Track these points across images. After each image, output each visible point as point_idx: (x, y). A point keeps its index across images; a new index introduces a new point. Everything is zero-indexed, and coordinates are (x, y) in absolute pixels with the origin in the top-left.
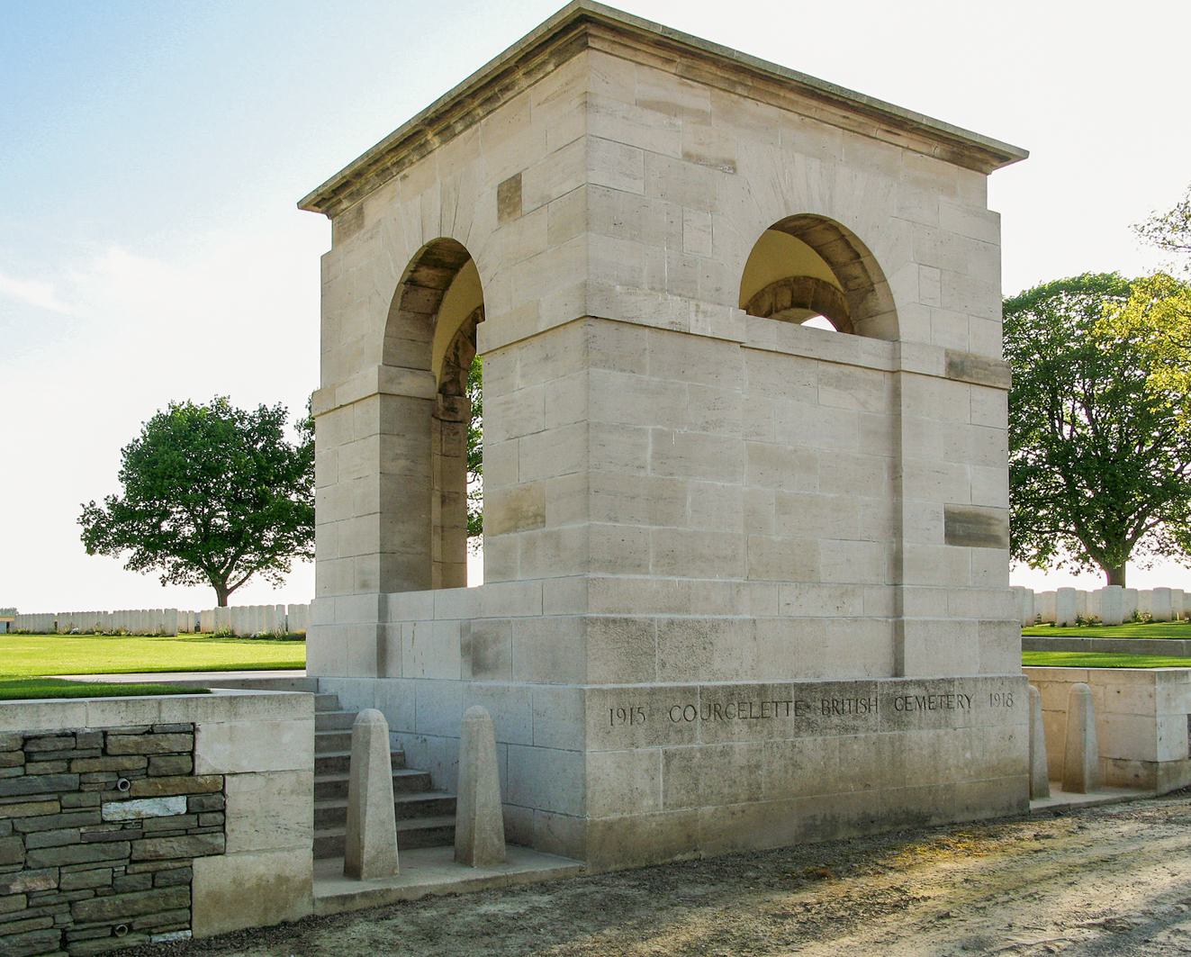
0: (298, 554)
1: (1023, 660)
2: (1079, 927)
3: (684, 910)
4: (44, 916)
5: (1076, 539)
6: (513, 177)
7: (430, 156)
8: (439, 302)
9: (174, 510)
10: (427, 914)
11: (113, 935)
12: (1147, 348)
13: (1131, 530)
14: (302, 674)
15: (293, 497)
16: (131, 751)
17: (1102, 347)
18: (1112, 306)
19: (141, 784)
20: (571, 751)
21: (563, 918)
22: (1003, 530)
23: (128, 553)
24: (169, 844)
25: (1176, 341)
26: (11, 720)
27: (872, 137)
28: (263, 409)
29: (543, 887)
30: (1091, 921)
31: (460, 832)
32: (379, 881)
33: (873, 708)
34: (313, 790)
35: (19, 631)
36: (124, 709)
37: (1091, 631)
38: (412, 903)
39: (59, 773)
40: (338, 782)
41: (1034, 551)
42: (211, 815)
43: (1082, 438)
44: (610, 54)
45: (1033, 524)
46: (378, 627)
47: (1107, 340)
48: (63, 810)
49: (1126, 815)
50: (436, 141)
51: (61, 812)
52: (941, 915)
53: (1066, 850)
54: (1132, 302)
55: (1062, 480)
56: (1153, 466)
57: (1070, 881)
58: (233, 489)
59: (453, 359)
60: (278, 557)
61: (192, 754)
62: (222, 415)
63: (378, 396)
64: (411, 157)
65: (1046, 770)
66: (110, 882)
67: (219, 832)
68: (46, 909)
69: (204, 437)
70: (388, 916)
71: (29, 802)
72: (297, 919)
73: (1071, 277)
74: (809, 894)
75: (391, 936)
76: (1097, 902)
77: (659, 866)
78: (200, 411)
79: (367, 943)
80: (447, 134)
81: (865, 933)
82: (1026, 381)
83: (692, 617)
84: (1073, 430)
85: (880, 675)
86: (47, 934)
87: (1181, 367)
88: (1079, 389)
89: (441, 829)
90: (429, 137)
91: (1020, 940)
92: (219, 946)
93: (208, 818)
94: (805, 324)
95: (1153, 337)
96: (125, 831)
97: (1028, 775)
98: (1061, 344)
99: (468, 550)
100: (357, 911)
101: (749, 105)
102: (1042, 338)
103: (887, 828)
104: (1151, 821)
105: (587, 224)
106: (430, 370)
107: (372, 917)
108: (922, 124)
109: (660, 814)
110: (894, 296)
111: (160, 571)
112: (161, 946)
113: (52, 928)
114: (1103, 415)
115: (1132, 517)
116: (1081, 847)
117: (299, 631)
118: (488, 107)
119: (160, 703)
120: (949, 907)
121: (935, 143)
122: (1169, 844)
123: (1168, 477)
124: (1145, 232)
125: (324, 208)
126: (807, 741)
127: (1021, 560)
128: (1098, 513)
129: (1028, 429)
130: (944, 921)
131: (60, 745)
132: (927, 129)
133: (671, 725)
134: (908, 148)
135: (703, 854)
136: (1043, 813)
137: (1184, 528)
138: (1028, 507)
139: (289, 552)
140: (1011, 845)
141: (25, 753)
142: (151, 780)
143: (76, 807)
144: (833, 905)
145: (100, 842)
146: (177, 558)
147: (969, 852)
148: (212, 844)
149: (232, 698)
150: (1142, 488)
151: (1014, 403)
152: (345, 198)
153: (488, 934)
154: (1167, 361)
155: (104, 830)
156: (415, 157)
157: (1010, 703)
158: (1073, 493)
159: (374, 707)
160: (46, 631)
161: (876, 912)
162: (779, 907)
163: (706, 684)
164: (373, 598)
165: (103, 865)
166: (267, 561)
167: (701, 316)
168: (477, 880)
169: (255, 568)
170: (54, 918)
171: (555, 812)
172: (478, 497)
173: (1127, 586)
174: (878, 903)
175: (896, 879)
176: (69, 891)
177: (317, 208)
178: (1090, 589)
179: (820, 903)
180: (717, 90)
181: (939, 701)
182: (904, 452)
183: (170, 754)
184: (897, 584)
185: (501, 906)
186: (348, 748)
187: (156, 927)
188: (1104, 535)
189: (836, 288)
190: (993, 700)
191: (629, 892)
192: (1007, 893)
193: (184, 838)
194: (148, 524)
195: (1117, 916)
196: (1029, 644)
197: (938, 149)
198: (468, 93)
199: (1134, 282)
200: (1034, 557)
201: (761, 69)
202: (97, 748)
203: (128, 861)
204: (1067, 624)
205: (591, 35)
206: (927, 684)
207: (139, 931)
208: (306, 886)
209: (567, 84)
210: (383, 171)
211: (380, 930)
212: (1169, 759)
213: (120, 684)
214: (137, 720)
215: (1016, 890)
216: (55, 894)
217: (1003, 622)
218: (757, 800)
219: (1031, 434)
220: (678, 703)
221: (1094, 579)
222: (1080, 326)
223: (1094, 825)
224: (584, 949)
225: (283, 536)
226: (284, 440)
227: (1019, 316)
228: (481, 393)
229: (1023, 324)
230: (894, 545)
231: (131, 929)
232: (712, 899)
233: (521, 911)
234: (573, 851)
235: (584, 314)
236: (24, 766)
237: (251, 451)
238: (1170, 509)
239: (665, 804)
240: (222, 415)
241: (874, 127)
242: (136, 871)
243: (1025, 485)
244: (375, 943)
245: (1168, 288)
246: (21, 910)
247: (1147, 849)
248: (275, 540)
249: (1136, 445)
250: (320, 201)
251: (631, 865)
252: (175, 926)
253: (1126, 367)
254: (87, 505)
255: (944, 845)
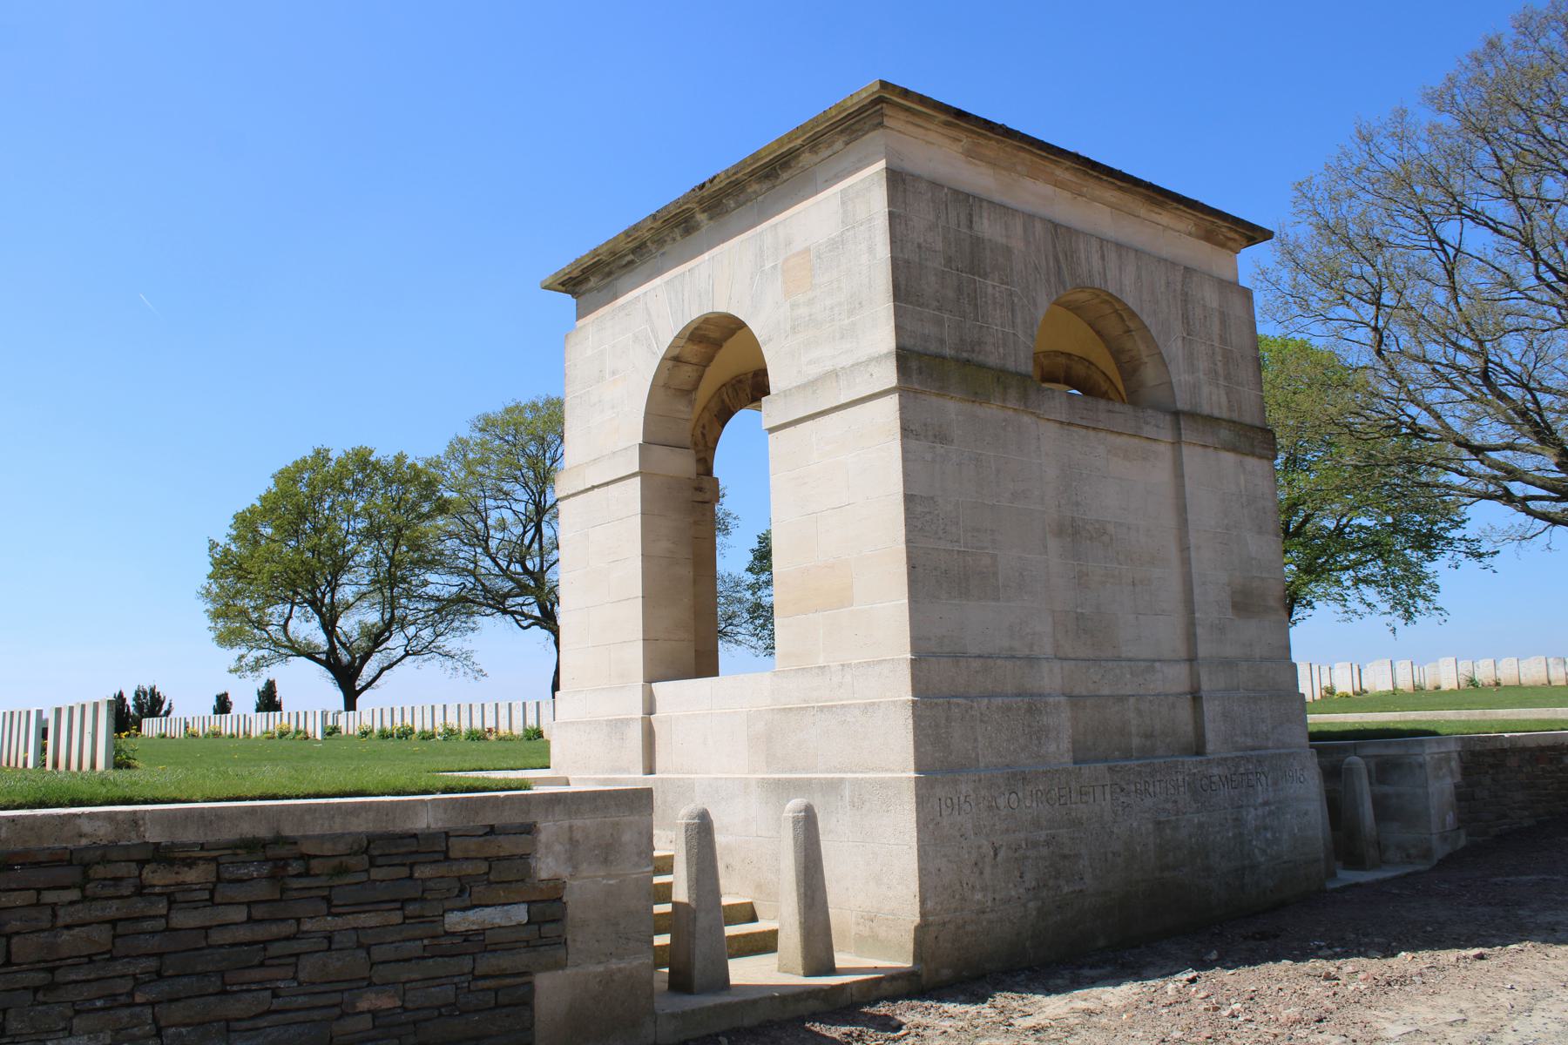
48: (407, 921)
51: (403, 923)
93: (548, 929)
155: (445, 941)
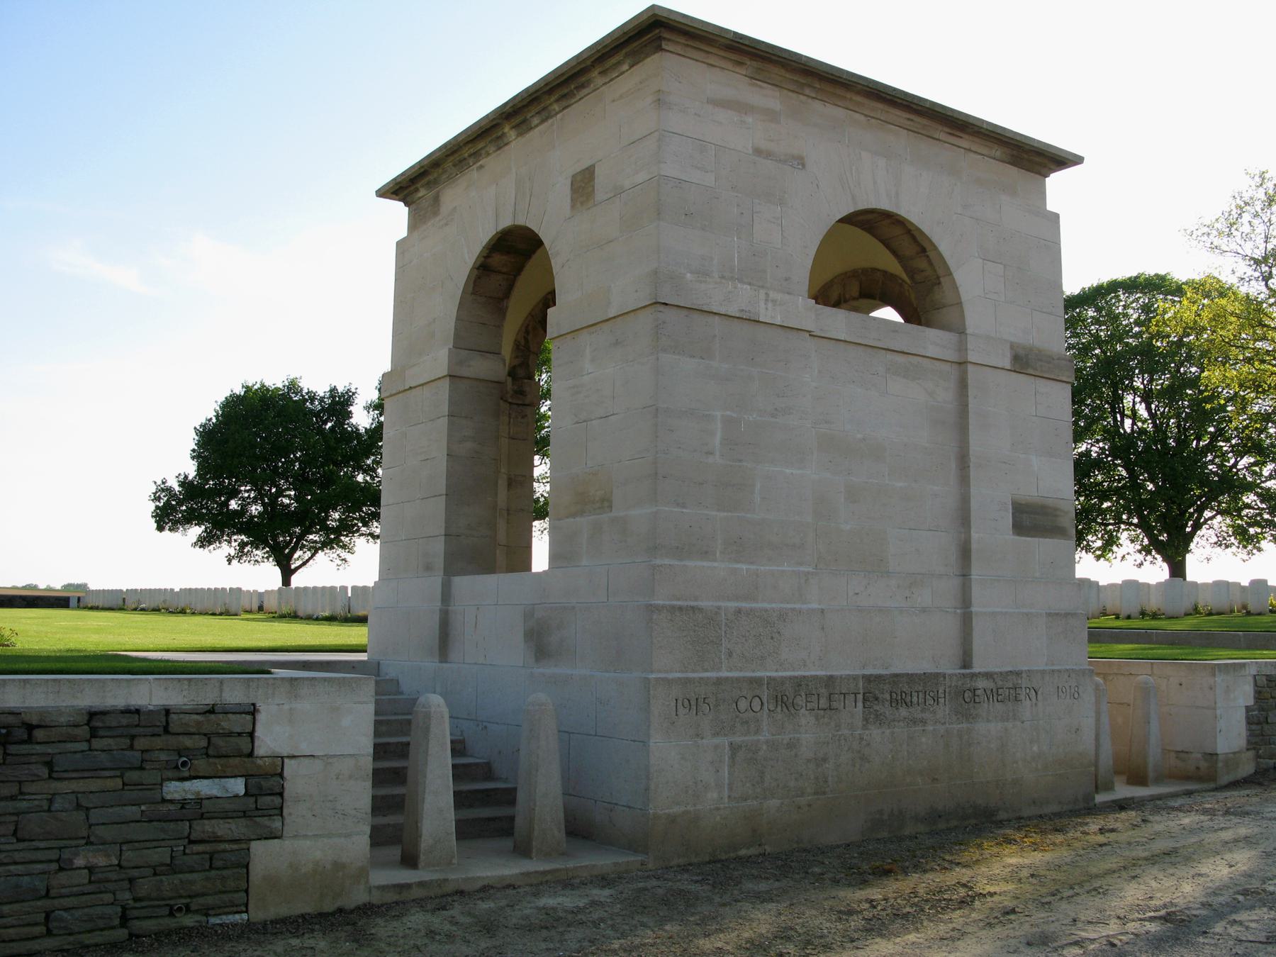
0: (362, 535)
1: (1089, 652)
2: (1141, 920)
3: (747, 906)
4: (106, 892)
5: (1139, 531)
6: (587, 169)
7: (506, 148)
8: (510, 287)
9: (243, 488)
10: (485, 905)
11: (171, 914)
12: (1200, 346)
13: (1190, 523)
14: (363, 657)
15: (360, 478)
16: (193, 730)
17: (1159, 344)
18: (1167, 306)
19: (201, 764)
20: (634, 741)
21: (624, 912)
22: (1069, 521)
23: (196, 531)
24: (227, 825)
25: (1227, 340)
26: (79, 695)
27: (937, 139)
28: (333, 390)
29: (604, 881)
30: (1152, 914)
31: (519, 822)
32: (436, 870)
33: (942, 700)
34: (371, 775)
35: (89, 606)
36: (186, 687)
37: (1154, 623)
38: (469, 893)
39: (122, 749)
40: (396, 768)
41: (1099, 543)
42: (269, 798)
43: (1143, 431)
44: (684, 56)
45: (1098, 516)
46: (440, 610)
47: (1163, 337)
48: (126, 788)
49: (1187, 807)
50: (512, 134)
51: (123, 789)
52: (1006, 911)
53: (1129, 844)
54: (1185, 302)
55: (1124, 473)
56: (1210, 461)
57: (1133, 874)
58: (300, 468)
59: (523, 342)
60: (342, 538)
61: (251, 735)
62: (293, 395)
63: (448, 378)
64: (487, 149)
65: (1111, 763)
66: (168, 861)
67: (277, 815)
68: (106, 885)
69: (274, 417)
70: (445, 906)
71: (92, 777)
72: (352, 906)
73: (1128, 275)
74: (875, 890)
75: (447, 927)
76: (1159, 895)
77: (723, 861)
78: (272, 391)
79: (423, 933)
80: (523, 127)
81: (932, 930)
82: (1088, 375)
83: (760, 605)
84: (1134, 424)
85: (948, 666)
86: (109, 910)
87: (1232, 365)
88: (1139, 384)
89: (500, 819)
90: (506, 129)
91: (1084, 934)
92: (275, 931)
94: (873, 314)
95: (1205, 336)
96: (184, 811)
97: (1093, 769)
98: (1120, 340)
99: (534, 534)
100: (413, 900)
101: (817, 105)
102: (1102, 334)
103: (954, 823)
104: (1211, 813)
105: (659, 214)
106: (499, 354)
107: (429, 907)
108: (982, 128)
109: (725, 808)
110: (960, 289)
111: (226, 549)
112: (217, 928)
113: (112, 904)
114: (1162, 410)
115: (1192, 510)
116: (1145, 840)
117: (361, 613)
118: (564, 103)
119: (221, 682)
120: (1015, 902)
121: (996, 147)
122: (1227, 835)
123: (1224, 472)
124: (1194, 236)
125: (401, 196)
126: (876, 734)
127: (1086, 552)
128: (1160, 506)
129: (1091, 421)
130: (1008, 917)
131: (124, 721)
132: (987, 132)
133: (737, 717)
134: (970, 150)
135: (768, 849)
136: (1108, 807)
137: (1240, 522)
138: (1092, 499)
139: (353, 533)
140: (1077, 839)
141: (91, 728)
142: (211, 760)
143: (138, 785)
144: (899, 901)
145: (159, 821)
146: (243, 537)
147: (1035, 847)
148: (269, 827)
149: (292, 680)
150: (1200, 482)
151: (1077, 397)
152: (422, 186)
153: (547, 928)
154: (1220, 359)
155: (164, 808)
156: (491, 149)
157: (1076, 696)
158: (1135, 485)
159: (434, 693)
160: (115, 607)
161: (942, 908)
162: (844, 904)
163: (774, 674)
164: (437, 580)
165: (163, 843)
166: (331, 541)
167: (770, 305)
168: (536, 872)
169: (320, 548)
170: (114, 894)
171: (616, 804)
172: (544, 481)
173: (1189, 577)
174: (945, 899)
175: (963, 874)
176: (129, 868)
177: (394, 196)
178: (1153, 581)
179: (886, 899)
180: (785, 91)
181: (1007, 694)
182: (972, 442)
183: (230, 734)
184: (965, 575)
185: (560, 900)
186: (407, 734)
187: (213, 909)
188: (1165, 529)
189: (903, 281)
190: (1061, 693)
191: (693, 887)
192: (1072, 888)
193: (243, 820)
194: (216, 503)
195: (1178, 908)
196: (1096, 636)
197: (998, 152)
198: (545, 89)
199: (1186, 283)
200: (1099, 549)
201: (828, 73)
202: (159, 726)
203: (187, 840)
204: (1132, 616)
205: (665, 39)
206: (995, 676)
207: (197, 912)
208: (362, 874)
209: (641, 83)
210: (460, 161)
211: (436, 921)
212: (1227, 751)
213: (183, 662)
214: (200, 699)
215: (1081, 884)
216: (116, 871)
217: (1069, 614)
218: (824, 793)
219: (1094, 427)
220: (744, 693)
221: (1156, 572)
222: (1138, 323)
223: (1158, 818)
224: (645, 945)
225: (348, 516)
226: (353, 421)
227: (1080, 312)
228: (550, 376)
229: (1084, 320)
230: (963, 535)
231: (188, 909)
232: (776, 895)
233: (581, 905)
234: (633, 845)
235: (654, 301)
236: (89, 741)
237: (321, 431)
238: (1226, 503)
239: (729, 797)
240: (293, 395)
241: (937, 129)
242: (194, 852)
243: (1090, 477)
244: (431, 934)
245: (1217, 290)
246: (84, 885)
247: (1207, 840)
248: (340, 520)
249: (1194, 440)
250: (397, 190)
251: (695, 860)
252: (232, 909)
253: (1182, 364)
254: (159, 482)
255: (1011, 840)
